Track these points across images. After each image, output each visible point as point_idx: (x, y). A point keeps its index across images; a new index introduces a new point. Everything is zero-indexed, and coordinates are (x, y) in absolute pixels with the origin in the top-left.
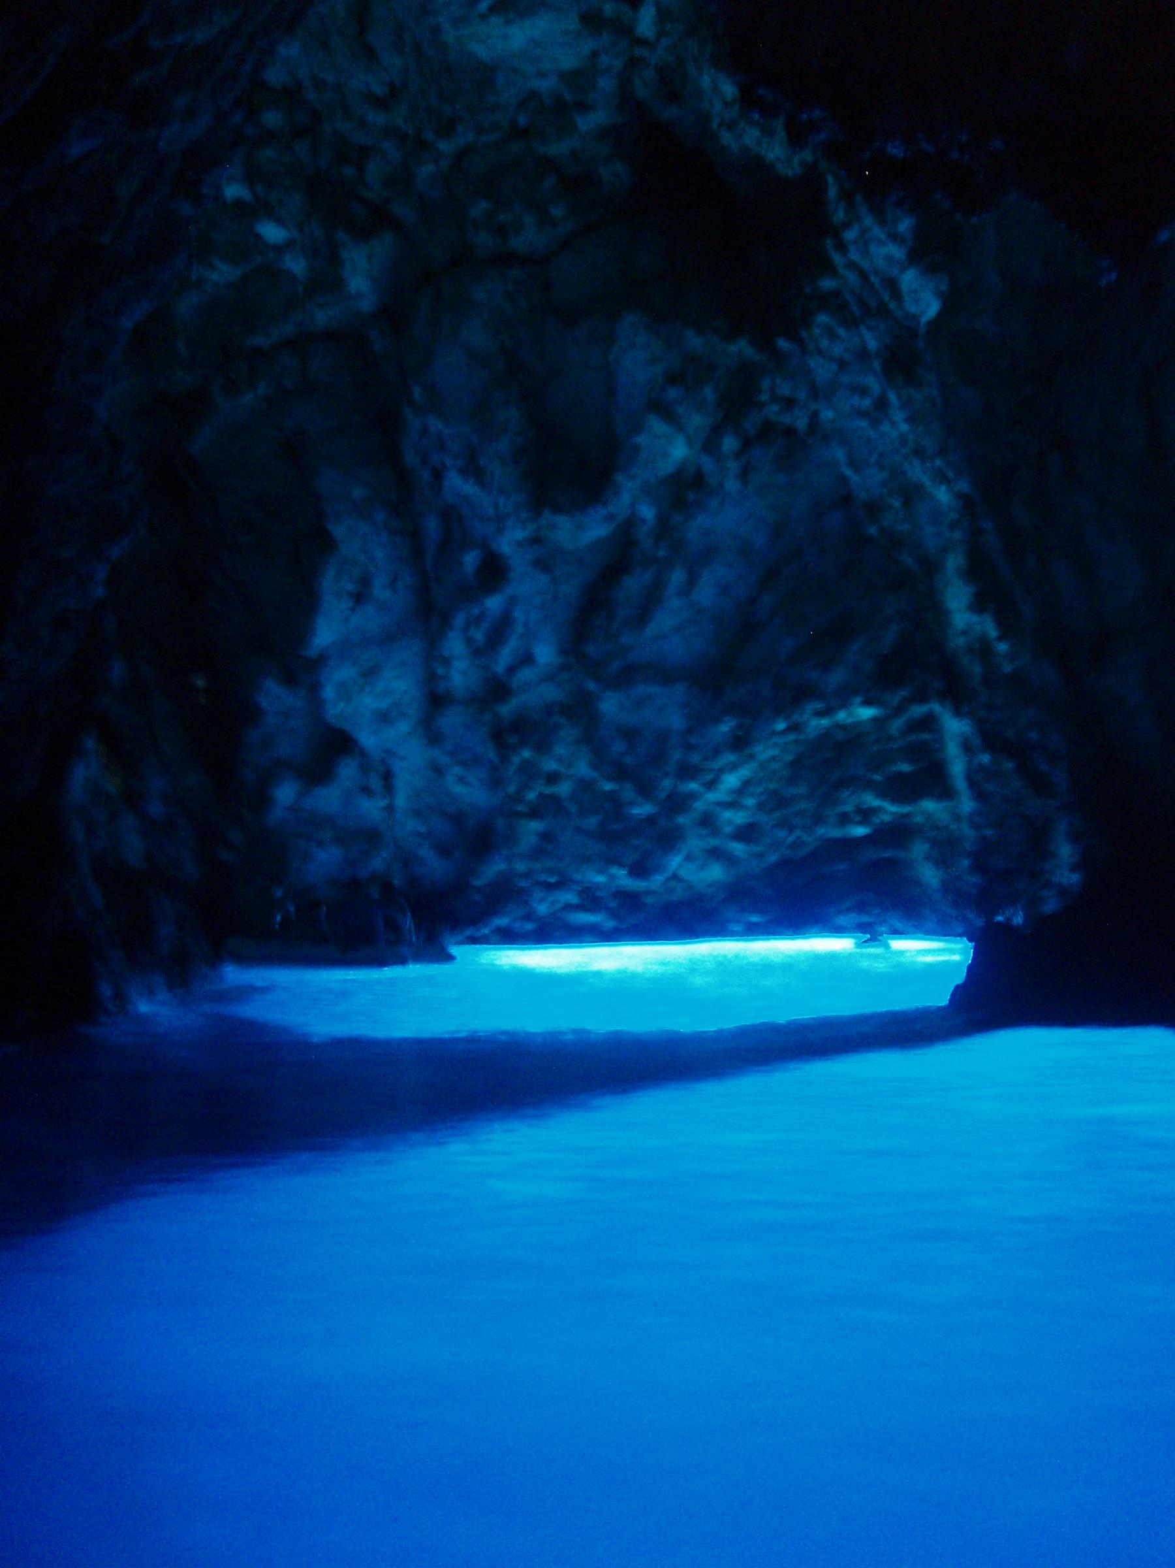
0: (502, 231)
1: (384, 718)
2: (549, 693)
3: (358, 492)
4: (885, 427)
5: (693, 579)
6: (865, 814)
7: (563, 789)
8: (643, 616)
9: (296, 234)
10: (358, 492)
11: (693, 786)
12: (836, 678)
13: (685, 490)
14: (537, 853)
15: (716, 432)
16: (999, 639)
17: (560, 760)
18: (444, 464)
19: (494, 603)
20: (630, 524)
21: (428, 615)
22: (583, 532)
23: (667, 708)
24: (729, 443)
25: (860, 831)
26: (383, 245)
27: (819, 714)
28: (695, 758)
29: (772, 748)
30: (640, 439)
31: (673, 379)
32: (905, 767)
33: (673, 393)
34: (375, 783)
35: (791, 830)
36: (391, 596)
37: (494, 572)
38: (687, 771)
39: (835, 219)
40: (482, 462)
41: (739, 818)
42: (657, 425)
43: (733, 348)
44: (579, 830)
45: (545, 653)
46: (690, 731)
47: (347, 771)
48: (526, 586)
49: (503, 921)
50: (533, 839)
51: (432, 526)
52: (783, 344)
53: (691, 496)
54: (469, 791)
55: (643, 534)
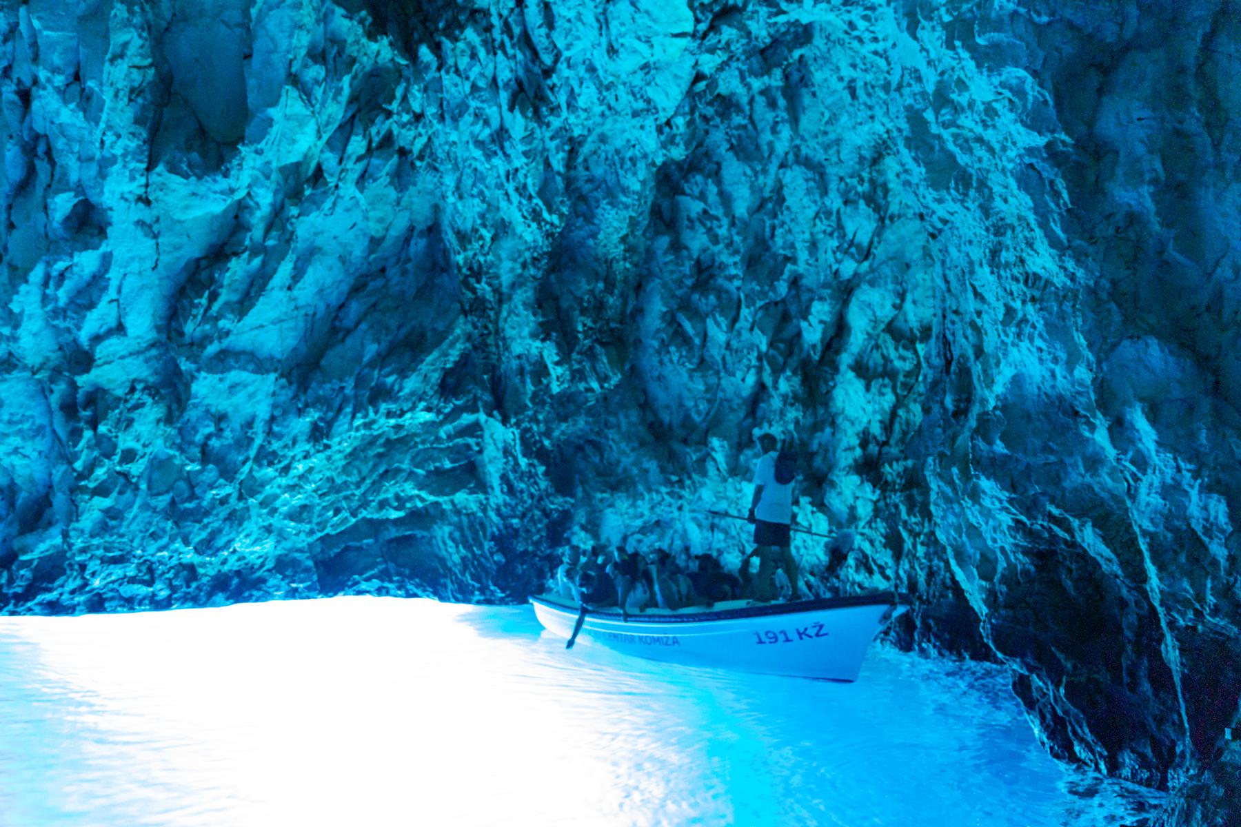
2: (140, 370)
4: (497, 161)
5: (297, 275)
6: (401, 501)
7: (136, 468)
8: (243, 305)
11: (270, 472)
12: (412, 384)
13: (302, 184)
14: (103, 528)
15: (345, 130)
16: (557, 363)
18: (35, 81)
19: (87, 261)
22: (194, 204)
23: (248, 397)
24: (357, 145)
25: (394, 515)
27: (389, 415)
28: (276, 445)
29: (347, 435)
30: (273, 112)
31: (317, 55)
32: (448, 465)
33: (316, 72)
35: (337, 512)
37: (88, 223)
38: (266, 457)
40: (90, 84)
41: (298, 500)
42: (291, 102)
43: (374, 47)
44: (145, 507)
45: (141, 325)
46: (273, 419)
50: (97, 515)
52: (425, 53)
53: (308, 192)
55: (257, 219)
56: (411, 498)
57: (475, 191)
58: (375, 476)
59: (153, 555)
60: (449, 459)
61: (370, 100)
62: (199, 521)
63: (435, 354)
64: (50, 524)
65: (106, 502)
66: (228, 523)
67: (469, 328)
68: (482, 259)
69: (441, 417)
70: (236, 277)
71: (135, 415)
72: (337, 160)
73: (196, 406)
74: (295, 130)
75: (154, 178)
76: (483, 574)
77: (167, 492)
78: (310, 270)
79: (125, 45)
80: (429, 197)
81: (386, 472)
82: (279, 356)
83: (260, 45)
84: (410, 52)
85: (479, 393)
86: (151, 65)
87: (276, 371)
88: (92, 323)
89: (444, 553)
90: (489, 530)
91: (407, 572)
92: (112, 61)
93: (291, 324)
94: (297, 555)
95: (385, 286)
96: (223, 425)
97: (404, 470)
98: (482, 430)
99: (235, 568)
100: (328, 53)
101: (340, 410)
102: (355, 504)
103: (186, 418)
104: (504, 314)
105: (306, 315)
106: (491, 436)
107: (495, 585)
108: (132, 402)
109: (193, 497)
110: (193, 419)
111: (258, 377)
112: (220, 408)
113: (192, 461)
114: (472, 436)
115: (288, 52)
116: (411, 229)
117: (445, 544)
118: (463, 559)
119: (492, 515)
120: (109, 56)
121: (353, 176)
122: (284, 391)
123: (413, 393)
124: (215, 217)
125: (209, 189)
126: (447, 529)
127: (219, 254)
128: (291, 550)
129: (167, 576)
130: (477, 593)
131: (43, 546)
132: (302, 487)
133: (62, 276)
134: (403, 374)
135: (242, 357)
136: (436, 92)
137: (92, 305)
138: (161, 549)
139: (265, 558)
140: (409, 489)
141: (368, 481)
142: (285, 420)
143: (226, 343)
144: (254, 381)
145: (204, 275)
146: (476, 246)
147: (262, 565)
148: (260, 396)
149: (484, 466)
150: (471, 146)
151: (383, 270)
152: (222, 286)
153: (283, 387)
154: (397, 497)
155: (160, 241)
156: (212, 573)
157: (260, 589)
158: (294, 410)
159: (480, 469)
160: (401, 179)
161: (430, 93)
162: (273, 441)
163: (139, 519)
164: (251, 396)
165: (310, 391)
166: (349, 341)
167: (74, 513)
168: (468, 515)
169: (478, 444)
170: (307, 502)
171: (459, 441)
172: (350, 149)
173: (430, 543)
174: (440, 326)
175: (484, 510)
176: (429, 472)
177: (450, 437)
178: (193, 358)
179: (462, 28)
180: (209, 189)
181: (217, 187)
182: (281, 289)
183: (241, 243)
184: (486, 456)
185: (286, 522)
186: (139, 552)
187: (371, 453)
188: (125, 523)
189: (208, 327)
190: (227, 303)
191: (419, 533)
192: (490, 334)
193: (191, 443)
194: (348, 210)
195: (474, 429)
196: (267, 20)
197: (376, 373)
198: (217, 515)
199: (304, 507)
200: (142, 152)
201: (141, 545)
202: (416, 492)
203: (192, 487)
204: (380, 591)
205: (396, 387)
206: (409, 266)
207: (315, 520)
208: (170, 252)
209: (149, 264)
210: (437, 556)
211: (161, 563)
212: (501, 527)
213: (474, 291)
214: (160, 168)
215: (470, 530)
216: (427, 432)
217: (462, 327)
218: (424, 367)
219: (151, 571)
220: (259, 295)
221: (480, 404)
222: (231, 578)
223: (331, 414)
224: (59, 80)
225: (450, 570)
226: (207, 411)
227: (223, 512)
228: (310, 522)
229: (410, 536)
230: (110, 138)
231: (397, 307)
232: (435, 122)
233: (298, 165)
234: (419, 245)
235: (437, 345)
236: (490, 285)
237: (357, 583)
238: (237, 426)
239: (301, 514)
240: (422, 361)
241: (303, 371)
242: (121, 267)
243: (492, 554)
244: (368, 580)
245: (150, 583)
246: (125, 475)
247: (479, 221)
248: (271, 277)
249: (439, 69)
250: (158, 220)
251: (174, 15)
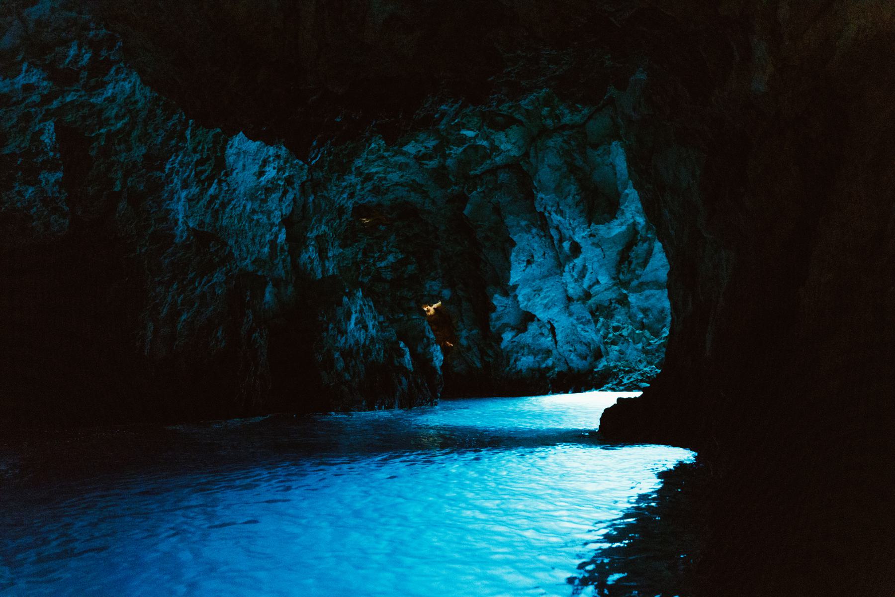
0: (558, 117)
1: (547, 307)
2: (612, 295)
3: (523, 223)
7: (625, 333)
9: (478, 132)
10: (523, 223)
17: (618, 321)
19: (578, 261)
20: (635, 224)
21: (560, 266)
26: (514, 132)
34: (545, 331)
36: (543, 260)
39: (61, 176)
45: (604, 280)
47: (533, 328)
48: (590, 255)
49: (610, 385)
51: (553, 232)
54: (591, 334)
64: (602, 356)
65: (617, 348)
71: (614, 312)
88: (586, 283)
131: (602, 364)
133: (573, 268)
137: (584, 276)
143: (641, 280)
167: (607, 353)
224: (554, 208)
230: (571, 222)
246: (621, 335)
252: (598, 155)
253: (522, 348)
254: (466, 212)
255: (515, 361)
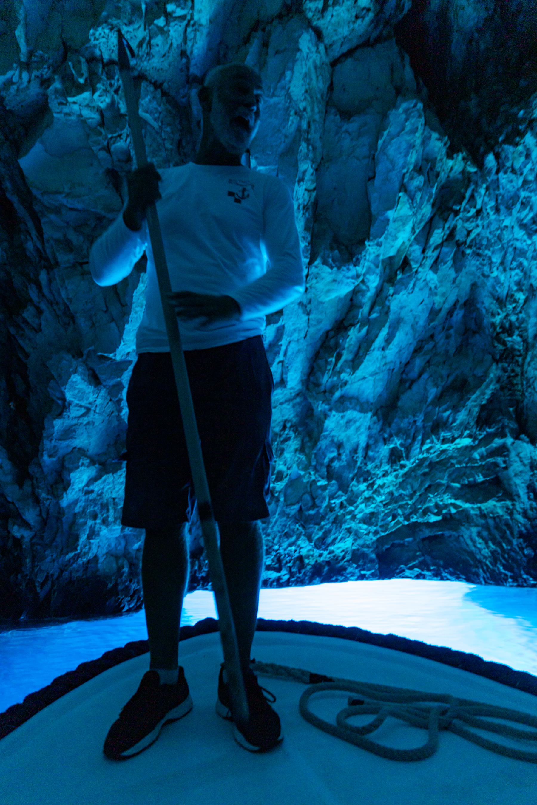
5: (389, 340)
8: (355, 363)
12: (462, 416)
13: (397, 270)
15: (429, 228)
24: (437, 236)
25: (433, 519)
30: (390, 214)
32: (480, 478)
43: (450, 163)
44: (283, 514)
46: (368, 447)
53: (399, 277)
55: (367, 299)
56: (446, 506)
57: (515, 264)
58: (422, 490)
59: (285, 550)
60: (482, 475)
61: (448, 201)
62: (318, 524)
63: (478, 393)
66: (334, 525)
67: (499, 372)
68: (513, 318)
69: (477, 442)
70: (352, 343)
71: (284, 446)
72: (421, 250)
73: (326, 437)
74: (400, 230)
75: (313, 270)
76: (515, 566)
77: (298, 502)
78: (398, 334)
79: (304, 172)
80: (471, 277)
81: (430, 486)
82: (372, 401)
83: (380, 168)
84: (480, 163)
85: (506, 422)
86: (315, 189)
87: (371, 411)
89: (473, 548)
90: (516, 530)
91: (441, 563)
92: (299, 181)
93: (380, 376)
94: (365, 549)
95: (434, 347)
96: (341, 451)
97: (443, 485)
98: (508, 450)
99: (327, 559)
100: (426, 167)
101: (414, 439)
102: (408, 511)
103: (319, 446)
104: (528, 359)
105: (389, 369)
106: (518, 455)
107: (527, 574)
108: (284, 436)
109: (314, 506)
110: (324, 447)
111: (362, 415)
112: (340, 438)
113: (323, 478)
114: (501, 455)
115: (403, 168)
116: (457, 301)
117: (474, 542)
118: (493, 552)
119: (520, 518)
120: (297, 179)
121: (429, 262)
122: (376, 426)
123: (461, 424)
124: (340, 299)
125: (344, 276)
126: (474, 530)
127: (341, 326)
128: (363, 546)
129: (289, 565)
130: (510, 580)
132: (374, 499)
134: (456, 409)
135: (353, 400)
136: (494, 190)
138: (290, 545)
139: (345, 552)
140: (448, 499)
141: (418, 494)
142: (376, 447)
144: (360, 418)
145: (332, 342)
146: (510, 307)
147: (344, 557)
148: (362, 430)
149: (510, 479)
150: (516, 229)
151: (432, 336)
152: (344, 349)
153: (375, 423)
154: (437, 506)
155: (311, 316)
156: (312, 562)
157: (342, 575)
158: (381, 440)
159: (505, 482)
160: (458, 264)
161: (491, 191)
162: (368, 463)
163: (278, 523)
164: (358, 429)
165: (393, 425)
166: (415, 387)
168: (494, 518)
169: (505, 462)
170: (375, 510)
171: (491, 460)
172: (432, 241)
173: (457, 539)
174: (479, 372)
175: (511, 514)
176: (463, 486)
177: (482, 458)
178: (326, 401)
179: (522, 135)
180: (344, 276)
181: (350, 274)
182: (379, 349)
183: (355, 317)
184: (511, 472)
185: (361, 525)
186: (276, 547)
187: (420, 472)
188: (271, 526)
189: (335, 378)
190: (346, 361)
191: (447, 533)
192: (517, 375)
193: (322, 464)
194: (421, 289)
195: (502, 451)
196: (389, 147)
197: (437, 409)
198: (328, 519)
199: (372, 514)
200: (308, 251)
201: (279, 542)
202: (453, 501)
203: (313, 499)
204: (418, 577)
205: (451, 420)
206: (452, 331)
207: (380, 524)
208: (315, 325)
209: (303, 334)
210: (466, 551)
211: (289, 555)
212: (528, 526)
213: (504, 343)
214: (317, 262)
215: (496, 530)
216: (461, 455)
217: (494, 372)
218: (469, 404)
219: (279, 561)
220: (366, 354)
221: (507, 430)
222: (324, 567)
223: (409, 441)
225: (480, 562)
226: (332, 441)
227: (331, 516)
228: (376, 525)
229: (436, 537)
231: (444, 362)
232: (491, 213)
233: (391, 258)
234: (459, 314)
235: (479, 386)
236: (521, 336)
237: (403, 571)
238: (347, 452)
239: (370, 519)
240: (469, 399)
241: (387, 410)
242: (288, 336)
243: (522, 549)
244: (411, 568)
245: (279, 570)
247: (515, 288)
248: (373, 341)
249: (497, 172)
250: (310, 302)
251: (322, 158)
252: (347, 131)
253: (105, 507)
254: (24, 162)
255: (90, 537)
